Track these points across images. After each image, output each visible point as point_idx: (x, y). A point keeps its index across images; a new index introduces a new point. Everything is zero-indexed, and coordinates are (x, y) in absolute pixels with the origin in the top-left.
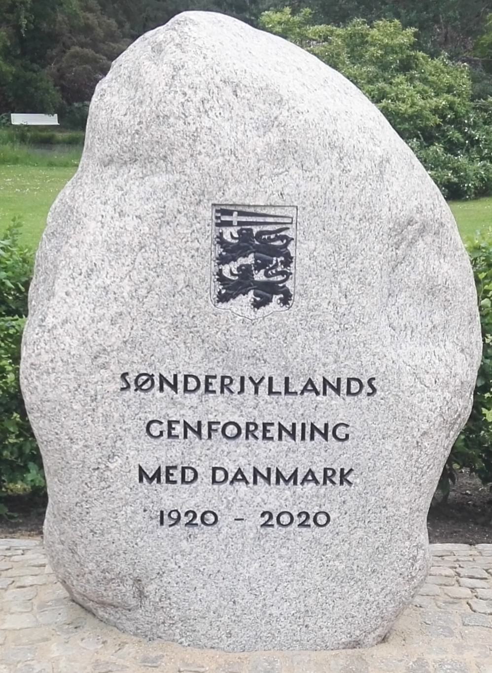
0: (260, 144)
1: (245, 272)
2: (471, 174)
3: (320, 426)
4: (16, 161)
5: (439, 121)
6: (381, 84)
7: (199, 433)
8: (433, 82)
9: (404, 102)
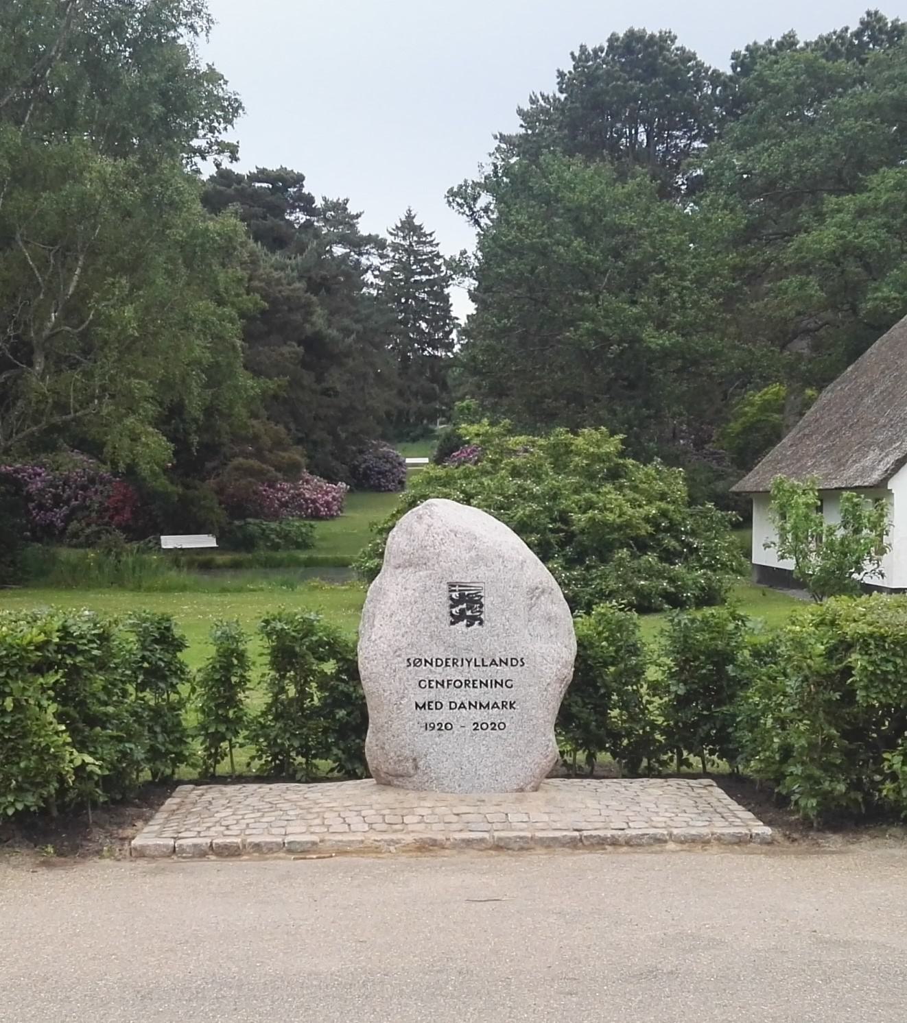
0: (468, 556)
1: (462, 611)
2: (690, 582)
3: (499, 681)
4: (183, 588)
5: (650, 529)
6: (588, 494)
7: (443, 685)
8: (646, 490)
9: (612, 512)
